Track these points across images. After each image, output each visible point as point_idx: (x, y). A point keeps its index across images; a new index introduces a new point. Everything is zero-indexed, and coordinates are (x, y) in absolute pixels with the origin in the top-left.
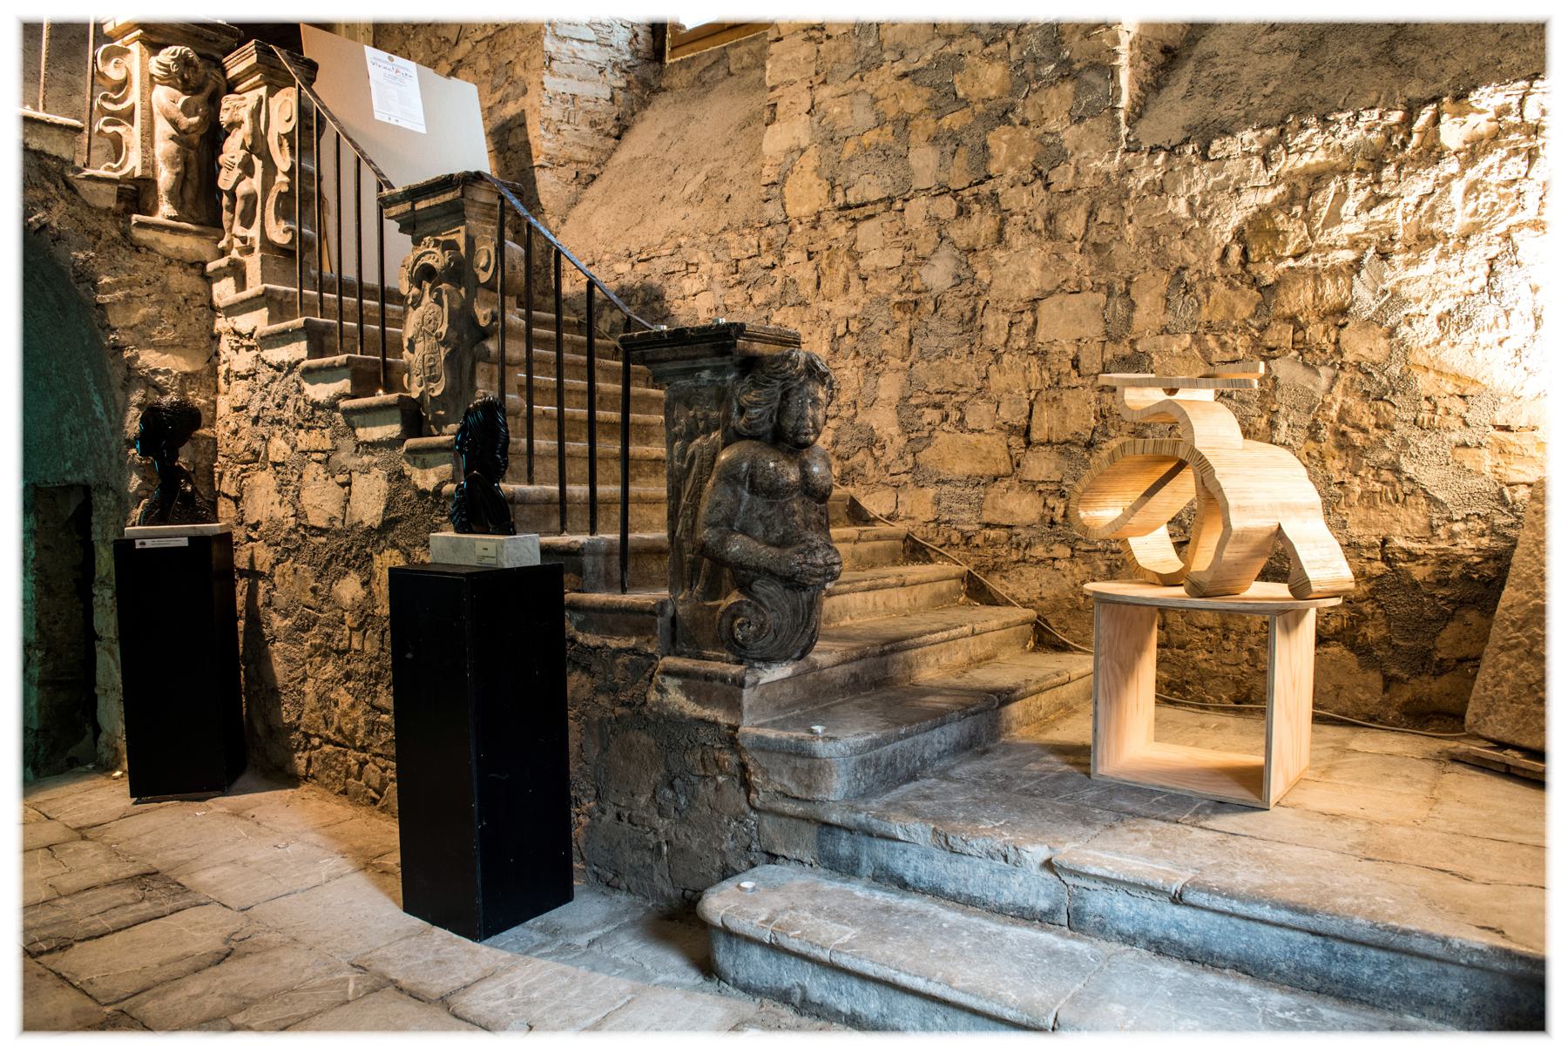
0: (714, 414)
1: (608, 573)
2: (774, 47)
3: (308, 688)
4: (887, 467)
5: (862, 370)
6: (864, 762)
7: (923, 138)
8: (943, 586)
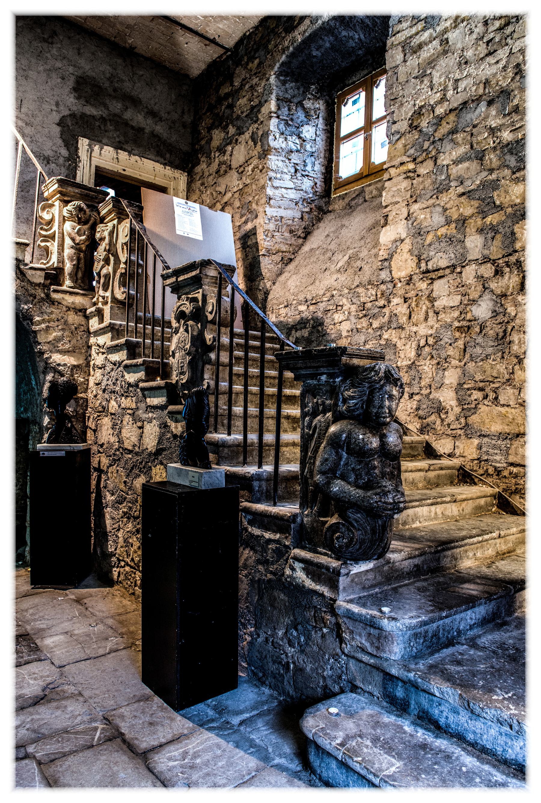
0: (328, 402)
1: (267, 491)
2: (387, 184)
3: (120, 534)
4: (449, 425)
5: (435, 367)
6: (416, 636)
7: (474, 230)
8: (482, 501)
